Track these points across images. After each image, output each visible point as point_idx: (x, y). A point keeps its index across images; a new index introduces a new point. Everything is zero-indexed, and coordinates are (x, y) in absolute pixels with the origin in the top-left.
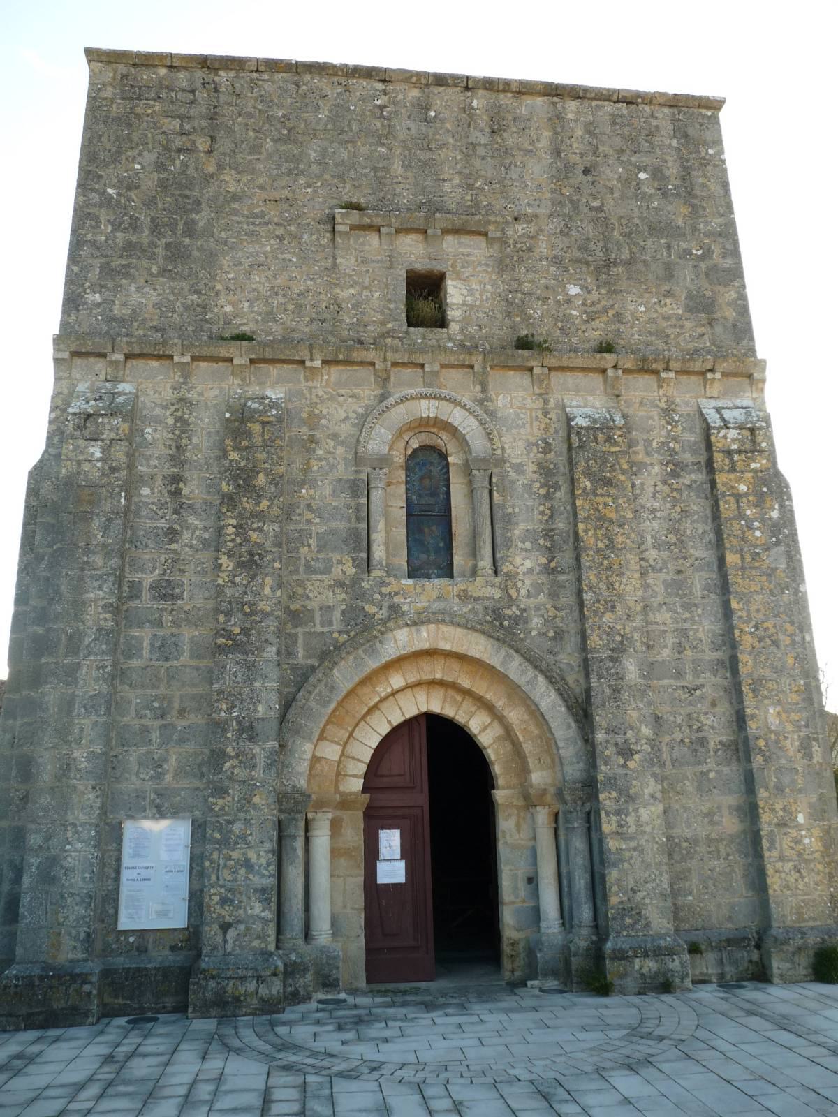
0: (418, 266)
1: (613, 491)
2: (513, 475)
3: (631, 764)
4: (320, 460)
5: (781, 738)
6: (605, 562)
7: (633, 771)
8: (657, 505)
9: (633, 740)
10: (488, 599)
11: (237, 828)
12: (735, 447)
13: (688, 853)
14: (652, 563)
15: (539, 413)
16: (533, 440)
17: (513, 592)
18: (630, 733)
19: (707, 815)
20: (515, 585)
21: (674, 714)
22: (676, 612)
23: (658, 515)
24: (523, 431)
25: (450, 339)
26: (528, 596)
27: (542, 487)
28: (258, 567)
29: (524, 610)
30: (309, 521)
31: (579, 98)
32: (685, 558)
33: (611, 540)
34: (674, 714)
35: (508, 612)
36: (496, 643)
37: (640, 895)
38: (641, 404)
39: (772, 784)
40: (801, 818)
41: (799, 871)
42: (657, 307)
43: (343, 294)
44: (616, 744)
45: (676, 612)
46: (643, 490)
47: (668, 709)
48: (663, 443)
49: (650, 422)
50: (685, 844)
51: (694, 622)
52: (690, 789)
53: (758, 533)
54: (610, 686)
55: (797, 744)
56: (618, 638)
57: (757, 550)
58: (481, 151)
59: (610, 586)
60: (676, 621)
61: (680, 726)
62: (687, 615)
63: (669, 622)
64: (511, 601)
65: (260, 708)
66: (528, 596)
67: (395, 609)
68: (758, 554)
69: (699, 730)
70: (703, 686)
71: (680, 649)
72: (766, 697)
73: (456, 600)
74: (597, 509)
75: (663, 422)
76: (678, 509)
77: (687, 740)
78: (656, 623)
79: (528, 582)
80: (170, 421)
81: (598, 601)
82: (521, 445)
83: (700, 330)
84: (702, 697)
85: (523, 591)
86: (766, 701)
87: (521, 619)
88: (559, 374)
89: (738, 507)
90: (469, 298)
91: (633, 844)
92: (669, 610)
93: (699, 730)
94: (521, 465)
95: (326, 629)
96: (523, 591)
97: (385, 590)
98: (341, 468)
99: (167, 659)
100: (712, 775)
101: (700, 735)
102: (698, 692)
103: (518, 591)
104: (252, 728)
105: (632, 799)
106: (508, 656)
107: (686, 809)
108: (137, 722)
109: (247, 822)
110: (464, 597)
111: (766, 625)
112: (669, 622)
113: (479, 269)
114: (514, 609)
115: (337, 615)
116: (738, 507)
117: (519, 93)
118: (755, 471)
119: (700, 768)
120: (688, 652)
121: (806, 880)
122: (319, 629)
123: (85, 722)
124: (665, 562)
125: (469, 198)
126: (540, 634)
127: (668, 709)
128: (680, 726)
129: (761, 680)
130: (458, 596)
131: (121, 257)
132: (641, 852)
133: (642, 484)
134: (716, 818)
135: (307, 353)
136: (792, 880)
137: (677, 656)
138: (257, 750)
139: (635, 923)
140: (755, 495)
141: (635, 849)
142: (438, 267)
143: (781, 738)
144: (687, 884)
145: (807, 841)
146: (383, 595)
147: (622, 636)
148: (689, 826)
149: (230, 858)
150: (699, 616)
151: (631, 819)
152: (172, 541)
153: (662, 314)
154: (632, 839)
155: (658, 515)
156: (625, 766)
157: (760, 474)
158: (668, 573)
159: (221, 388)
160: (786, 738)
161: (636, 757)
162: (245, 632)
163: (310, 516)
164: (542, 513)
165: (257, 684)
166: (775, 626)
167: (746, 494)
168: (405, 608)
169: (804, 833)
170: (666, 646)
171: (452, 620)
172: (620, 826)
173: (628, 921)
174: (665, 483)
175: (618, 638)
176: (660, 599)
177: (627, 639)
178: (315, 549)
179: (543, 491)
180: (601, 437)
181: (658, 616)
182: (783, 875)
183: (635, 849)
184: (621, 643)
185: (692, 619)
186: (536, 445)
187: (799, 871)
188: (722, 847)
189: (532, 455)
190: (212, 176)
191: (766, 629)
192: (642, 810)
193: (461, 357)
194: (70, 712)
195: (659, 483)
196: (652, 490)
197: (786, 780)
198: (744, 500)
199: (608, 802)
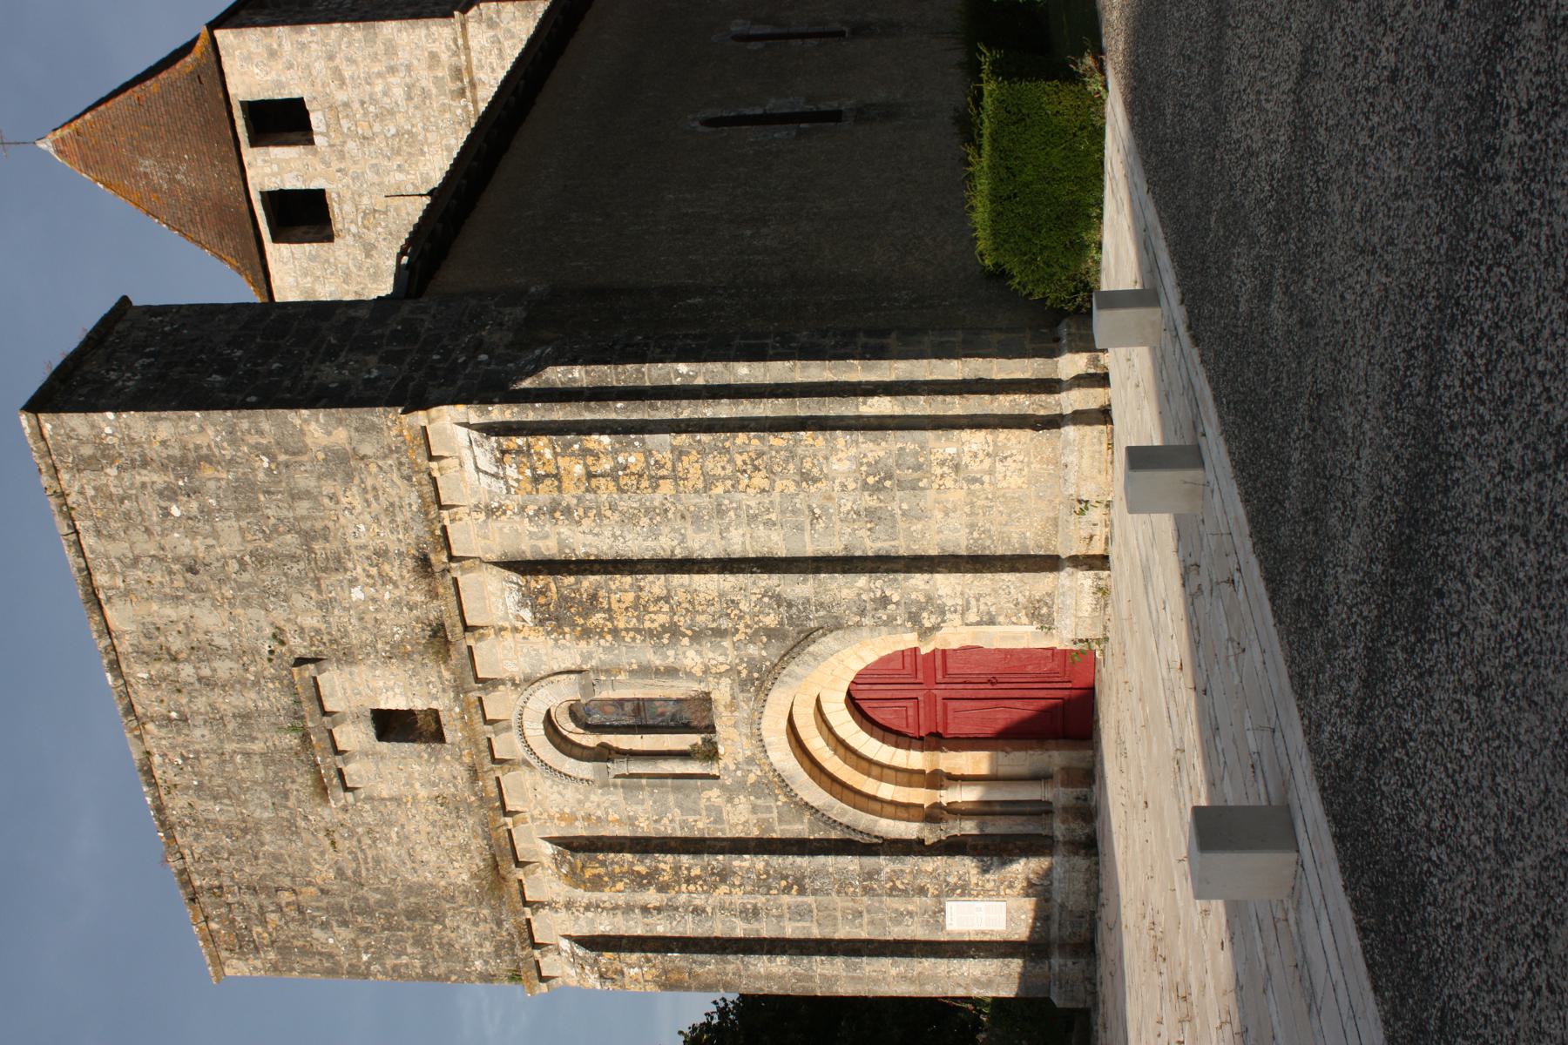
0: (372, 733)
1: (602, 593)
2: (594, 663)
3: (895, 598)
4: (607, 813)
5: (865, 460)
6: (684, 605)
7: (902, 597)
8: (607, 533)
9: (872, 595)
10: (732, 688)
11: (952, 880)
12: (528, 472)
13: (984, 532)
14: (676, 542)
15: (519, 636)
16: (552, 642)
17: (723, 668)
18: (864, 597)
19: (947, 514)
20: (716, 666)
21: (841, 534)
22: (730, 523)
23: (618, 533)
24: (542, 651)
25: (451, 710)
26: (726, 655)
27: (604, 638)
28: (724, 869)
29: (742, 660)
30: (671, 821)
31: (90, 574)
32: (666, 511)
33: (659, 599)
34: (841, 534)
35: (744, 674)
36: (777, 683)
37: (1021, 599)
38: (485, 537)
39: (916, 475)
40: (952, 450)
41: (1006, 458)
42: (355, 512)
43: (423, 793)
44: (876, 609)
45: (730, 523)
46: (590, 545)
47: (836, 539)
48: (530, 521)
49: (506, 530)
50: (976, 535)
51: (739, 507)
52: (919, 526)
53: (632, 459)
54: (817, 611)
55: (871, 445)
56: (766, 600)
57: (652, 462)
58: (206, 672)
59: (710, 603)
60: (738, 526)
61: (854, 530)
62: (732, 513)
63: (741, 531)
64: (732, 671)
65: (851, 868)
66: (726, 655)
67: (750, 760)
68: (656, 462)
69: (858, 513)
70: (809, 507)
71: (770, 524)
72: (821, 470)
73: (736, 714)
74: (627, 609)
75: (503, 518)
76: (609, 513)
77: (869, 525)
78: (743, 543)
79: (711, 655)
80: (590, 915)
81: (728, 615)
82: (558, 653)
83: (373, 468)
84: (822, 507)
85: (721, 659)
86: (825, 470)
87: (753, 664)
88: (467, 615)
89: (602, 475)
90: (397, 691)
91: (973, 602)
92: (727, 529)
93: (858, 513)
94: (582, 655)
95: (775, 811)
96: (721, 659)
97: (732, 767)
98: (613, 798)
99: (811, 911)
100: (905, 506)
101: (863, 513)
102: (817, 511)
103: (722, 664)
104: (868, 873)
105: (929, 599)
106: (789, 675)
107: (940, 532)
108: (865, 927)
109: (947, 874)
110: (733, 706)
111: (739, 463)
112: (741, 531)
113: (358, 680)
114: (740, 668)
115: (759, 802)
116: (602, 475)
117: (109, 633)
118: (555, 455)
119: (898, 517)
120: (773, 517)
121: (1014, 452)
122: (775, 814)
123: (868, 969)
124: (673, 530)
125: (271, 685)
126: (765, 646)
127: (836, 539)
128: (854, 530)
129: (802, 474)
130: (732, 712)
131: (431, 949)
132: (980, 595)
133: (584, 545)
134: (950, 505)
135: (500, 830)
136: (1014, 465)
137: (779, 526)
138: (888, 870)
139: (1046, 604)
140: (584, 457)
141: (978, 600)
142: (368, 714)
143: (865, 460)
144: (1014, 535)
145: (975, 448)
146: (738, 769)
147: (764, 596)
148: (956, 530)
149: (977, 884)
150: (731, 503)
151: (950, 603)
152: (704, 911)
153: (363, 508)
154: (968, 603)
155: (618, 533)
156: (897, 604)
157: (558, 450)
158: (686, 529)
159: (549, 881)
160: (865, 456)
161: (888, 593)
162: (785, 877)
163: (665, 821)
164: (634, 639)
165: (831, 870)
166: (741, 454)
167: (586, 466)
168: (748, 753)
169: (966, 449)
170: (769, 536)
171: (755, 722)
172: (955, 611)
173: (1044, 610)
174: (579, 523)
175: (766, 600)
176: (716, 537)
177: (766, 591)
178: (697, 817)
179: (609, 638)
180: (542, 600)
181: (735, 540)
182: (1008, 473)
183: (978, 600)
184: (771, 598)
185: (736, 509)
186: (556, 640)
187: (1006, 458)
188: (979, 503)
189: (568, 644)
190: (243, 754)
191: (745, 463)
192: (940, 593)
193: (473, 710)
194: (860, 978)
195: (580, 529)
196: (590, 537)
197: (911, 461)
198: (592, 469)
199: (933, 620)
